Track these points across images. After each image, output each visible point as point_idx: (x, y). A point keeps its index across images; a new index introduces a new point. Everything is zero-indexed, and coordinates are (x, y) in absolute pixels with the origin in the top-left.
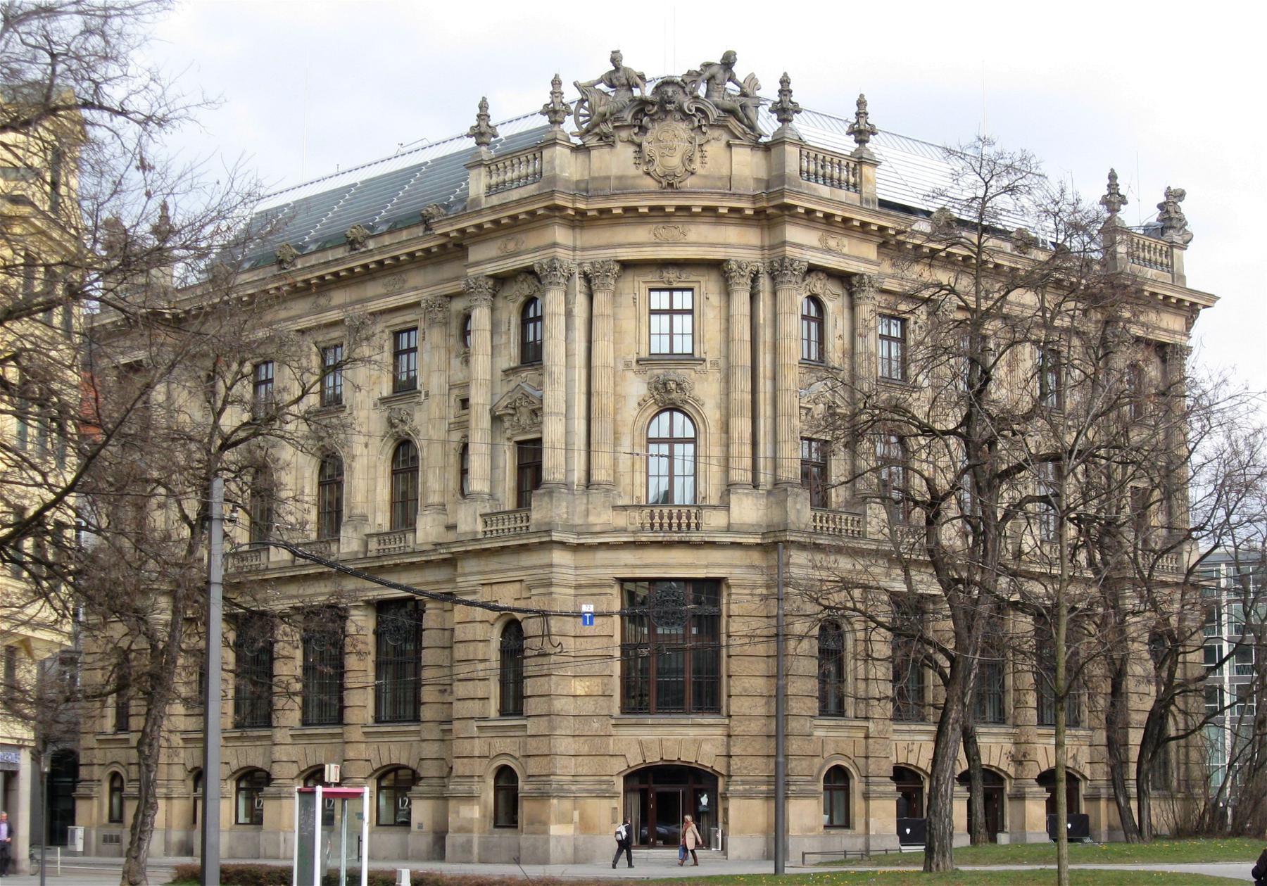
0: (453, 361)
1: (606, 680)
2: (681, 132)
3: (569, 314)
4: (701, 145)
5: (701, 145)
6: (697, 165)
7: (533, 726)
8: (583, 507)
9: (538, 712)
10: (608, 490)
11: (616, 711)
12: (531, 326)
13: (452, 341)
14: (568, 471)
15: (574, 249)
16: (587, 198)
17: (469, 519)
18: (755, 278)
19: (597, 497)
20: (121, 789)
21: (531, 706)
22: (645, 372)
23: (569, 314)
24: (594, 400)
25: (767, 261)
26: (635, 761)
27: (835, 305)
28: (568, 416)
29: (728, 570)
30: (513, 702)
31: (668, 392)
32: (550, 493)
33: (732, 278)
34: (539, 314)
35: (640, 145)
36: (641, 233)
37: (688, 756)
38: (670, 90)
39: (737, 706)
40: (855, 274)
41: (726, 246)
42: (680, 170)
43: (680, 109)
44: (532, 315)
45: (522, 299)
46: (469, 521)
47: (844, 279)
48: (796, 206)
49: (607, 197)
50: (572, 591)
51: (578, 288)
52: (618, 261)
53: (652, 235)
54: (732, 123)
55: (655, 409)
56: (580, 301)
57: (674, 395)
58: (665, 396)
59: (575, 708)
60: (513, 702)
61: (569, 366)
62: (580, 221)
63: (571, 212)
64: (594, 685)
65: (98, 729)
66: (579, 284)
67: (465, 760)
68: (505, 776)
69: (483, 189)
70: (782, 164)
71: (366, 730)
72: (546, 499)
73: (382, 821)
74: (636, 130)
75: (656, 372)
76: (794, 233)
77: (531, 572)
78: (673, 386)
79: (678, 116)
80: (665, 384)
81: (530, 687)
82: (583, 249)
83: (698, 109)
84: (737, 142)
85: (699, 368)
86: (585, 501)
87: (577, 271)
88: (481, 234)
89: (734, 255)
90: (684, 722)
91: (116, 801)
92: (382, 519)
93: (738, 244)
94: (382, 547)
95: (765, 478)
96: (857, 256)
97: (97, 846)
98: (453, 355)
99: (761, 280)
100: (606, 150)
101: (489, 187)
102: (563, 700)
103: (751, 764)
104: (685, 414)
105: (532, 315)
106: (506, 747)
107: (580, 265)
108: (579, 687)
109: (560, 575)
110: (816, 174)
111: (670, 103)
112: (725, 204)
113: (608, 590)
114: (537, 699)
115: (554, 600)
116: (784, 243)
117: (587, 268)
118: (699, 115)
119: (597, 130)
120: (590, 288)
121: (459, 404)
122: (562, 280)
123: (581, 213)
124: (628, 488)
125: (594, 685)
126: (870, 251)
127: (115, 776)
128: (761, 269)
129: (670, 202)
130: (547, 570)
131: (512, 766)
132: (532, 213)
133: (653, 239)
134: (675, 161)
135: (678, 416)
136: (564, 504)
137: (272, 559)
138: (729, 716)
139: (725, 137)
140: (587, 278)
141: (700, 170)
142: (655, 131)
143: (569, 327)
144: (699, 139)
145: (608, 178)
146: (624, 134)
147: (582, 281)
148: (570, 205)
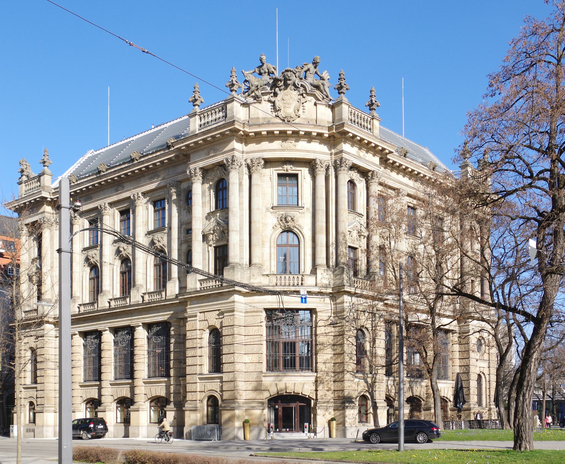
0: (182, 212)
1: (260, 355)
2: (294, 96)
3: (240, 184)
4: (303, 103)
5: (303, 103)
6: (301, 112)
7: (226, 377)
8: (248, 275)
9: (229, 370)
10: (260, 267)
11: (264, 370)
12: (221, 192)
13: (182, 203)
14: (242, 258)
15: (243, 152)
16: (250, 126)
17: (193, 282)
18: (327, 169)
19: (254, 270)
20: (34, 409)
21: (225, 368)
22: (276, 213)
23: (240, 184)
24: (253, 225)
25: (333, 160)
26: (273, 391)
27: (361, 185)
28: (241, 234)
29: (316, 305)
30: (217, 365)
31: (287, 222)
32: (233, 268)
33: (317, 168)
34: (224, 186)
35: (274, 103)
36: (277, 144)
37: (298, 390)
38: (289, 74)
39: (321, 366)
40: (370, 171)
41: (314, 152)
42: (293, 115)
43: (294, 85)
44: (221, 187)
45: (216, 179)
46: (194, 283)
47: (364, 173)
48: (349, 132)
49: (259, 125)
50: (243, 314)
51: (244, 172)
52: (263, 159)
53: (280, 146)
54: (317, 93)
55: (281, 230)
56: (246, 178)
57: (289, 224)
58: (286, 224)
59: (245, 368)
60: (217, 365)
61: (241, 209)
62: (246, 139)
63: (241, 133)
64: (255, 358)
65: (23, 383)
66: (245, 170)
67: (193, 393)
68: (213, 401)
69: (197, 127)
70: (341, 114)
71: (144, 381)
72: (231, 271)
73: (152, 421)
74: (272, 95)
75: (281, 213)
76: (346, 147)
77: (224, 305)
78: (290, 219)
79: (293, 87)
80: (285, 218)
81: (225, 359)
82: (248, 153)
83: (302, 86)
84: (319, 102)
85: (300, 211)
86: (249, 272)
87: (244, 163)
88: (197, 148)
89: (318, 157)
90: (296, 374)
91: (31, 414)
92: (151, 287)
93: (319, 151)
94: (151, 298)
95: (332, 262)
96: (371, 161)
97: (24, 434)
98: (182, 209)
99: (330, 170)
100: (257, 105)
101: (201, 126)
102: (240, 365)
103: (326, 394)
104: (294, 233)
105: (221, 187)
106: (215, 386)
107: (245, 160)
108: (247, 359)
109: (237, 306)
110: (354, 122)
111: (289, 80)
112: (315, 131)
113: (260, 314)
114: (228, 365)
115: (236, 318)
116: (342, 151)
117: (249, 162)
118: (302, 88)
119: (253, 94)
120: (250, 172)
121: (185, 231)
122: (237, 167)
123: (246, 135)
124: (269, 267)
125: (255, 358)
126: (376, 160)
127: (31, 404)
128: (331, 165)
129: (290, 129)
130: (232, 304)
131: (216, 395)
132: (222, 134)
133: (280, 148)
134: (290, 111)
135: (290, 234)
136: (239, 273)
137: (99, 306)
138: (316, 372)
139: (314, 100)
140: (249, 168)
141: (302, 116)
142: (281, 94)
143: (241, 190)
144: (303, 100)
145: (258, 118)
146: (266, 98)
147: (246, 169)
148: (242, 129)
